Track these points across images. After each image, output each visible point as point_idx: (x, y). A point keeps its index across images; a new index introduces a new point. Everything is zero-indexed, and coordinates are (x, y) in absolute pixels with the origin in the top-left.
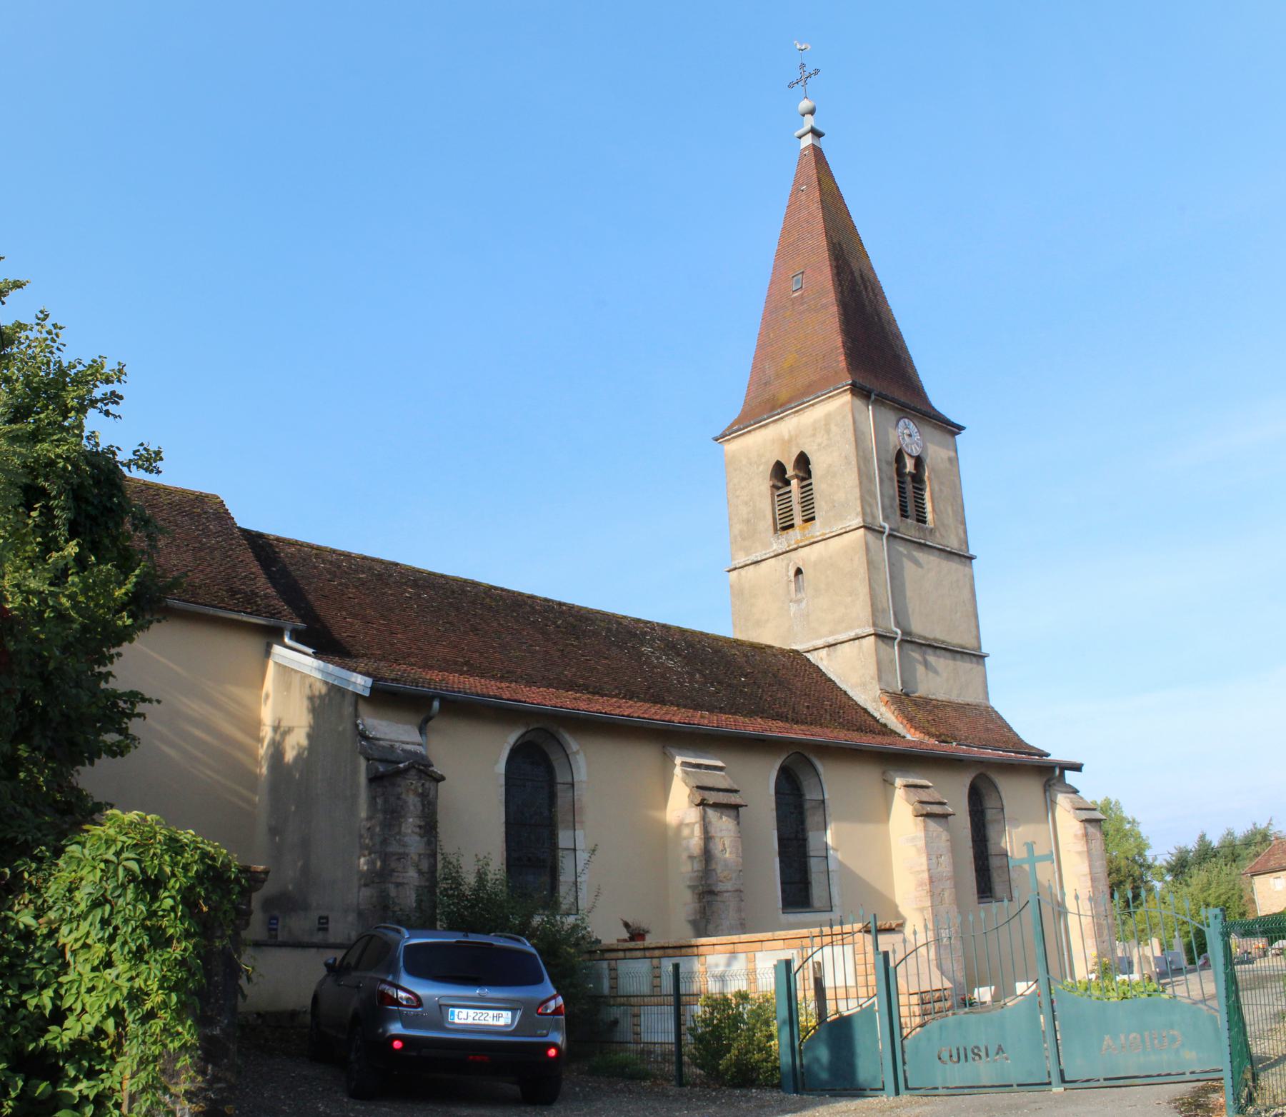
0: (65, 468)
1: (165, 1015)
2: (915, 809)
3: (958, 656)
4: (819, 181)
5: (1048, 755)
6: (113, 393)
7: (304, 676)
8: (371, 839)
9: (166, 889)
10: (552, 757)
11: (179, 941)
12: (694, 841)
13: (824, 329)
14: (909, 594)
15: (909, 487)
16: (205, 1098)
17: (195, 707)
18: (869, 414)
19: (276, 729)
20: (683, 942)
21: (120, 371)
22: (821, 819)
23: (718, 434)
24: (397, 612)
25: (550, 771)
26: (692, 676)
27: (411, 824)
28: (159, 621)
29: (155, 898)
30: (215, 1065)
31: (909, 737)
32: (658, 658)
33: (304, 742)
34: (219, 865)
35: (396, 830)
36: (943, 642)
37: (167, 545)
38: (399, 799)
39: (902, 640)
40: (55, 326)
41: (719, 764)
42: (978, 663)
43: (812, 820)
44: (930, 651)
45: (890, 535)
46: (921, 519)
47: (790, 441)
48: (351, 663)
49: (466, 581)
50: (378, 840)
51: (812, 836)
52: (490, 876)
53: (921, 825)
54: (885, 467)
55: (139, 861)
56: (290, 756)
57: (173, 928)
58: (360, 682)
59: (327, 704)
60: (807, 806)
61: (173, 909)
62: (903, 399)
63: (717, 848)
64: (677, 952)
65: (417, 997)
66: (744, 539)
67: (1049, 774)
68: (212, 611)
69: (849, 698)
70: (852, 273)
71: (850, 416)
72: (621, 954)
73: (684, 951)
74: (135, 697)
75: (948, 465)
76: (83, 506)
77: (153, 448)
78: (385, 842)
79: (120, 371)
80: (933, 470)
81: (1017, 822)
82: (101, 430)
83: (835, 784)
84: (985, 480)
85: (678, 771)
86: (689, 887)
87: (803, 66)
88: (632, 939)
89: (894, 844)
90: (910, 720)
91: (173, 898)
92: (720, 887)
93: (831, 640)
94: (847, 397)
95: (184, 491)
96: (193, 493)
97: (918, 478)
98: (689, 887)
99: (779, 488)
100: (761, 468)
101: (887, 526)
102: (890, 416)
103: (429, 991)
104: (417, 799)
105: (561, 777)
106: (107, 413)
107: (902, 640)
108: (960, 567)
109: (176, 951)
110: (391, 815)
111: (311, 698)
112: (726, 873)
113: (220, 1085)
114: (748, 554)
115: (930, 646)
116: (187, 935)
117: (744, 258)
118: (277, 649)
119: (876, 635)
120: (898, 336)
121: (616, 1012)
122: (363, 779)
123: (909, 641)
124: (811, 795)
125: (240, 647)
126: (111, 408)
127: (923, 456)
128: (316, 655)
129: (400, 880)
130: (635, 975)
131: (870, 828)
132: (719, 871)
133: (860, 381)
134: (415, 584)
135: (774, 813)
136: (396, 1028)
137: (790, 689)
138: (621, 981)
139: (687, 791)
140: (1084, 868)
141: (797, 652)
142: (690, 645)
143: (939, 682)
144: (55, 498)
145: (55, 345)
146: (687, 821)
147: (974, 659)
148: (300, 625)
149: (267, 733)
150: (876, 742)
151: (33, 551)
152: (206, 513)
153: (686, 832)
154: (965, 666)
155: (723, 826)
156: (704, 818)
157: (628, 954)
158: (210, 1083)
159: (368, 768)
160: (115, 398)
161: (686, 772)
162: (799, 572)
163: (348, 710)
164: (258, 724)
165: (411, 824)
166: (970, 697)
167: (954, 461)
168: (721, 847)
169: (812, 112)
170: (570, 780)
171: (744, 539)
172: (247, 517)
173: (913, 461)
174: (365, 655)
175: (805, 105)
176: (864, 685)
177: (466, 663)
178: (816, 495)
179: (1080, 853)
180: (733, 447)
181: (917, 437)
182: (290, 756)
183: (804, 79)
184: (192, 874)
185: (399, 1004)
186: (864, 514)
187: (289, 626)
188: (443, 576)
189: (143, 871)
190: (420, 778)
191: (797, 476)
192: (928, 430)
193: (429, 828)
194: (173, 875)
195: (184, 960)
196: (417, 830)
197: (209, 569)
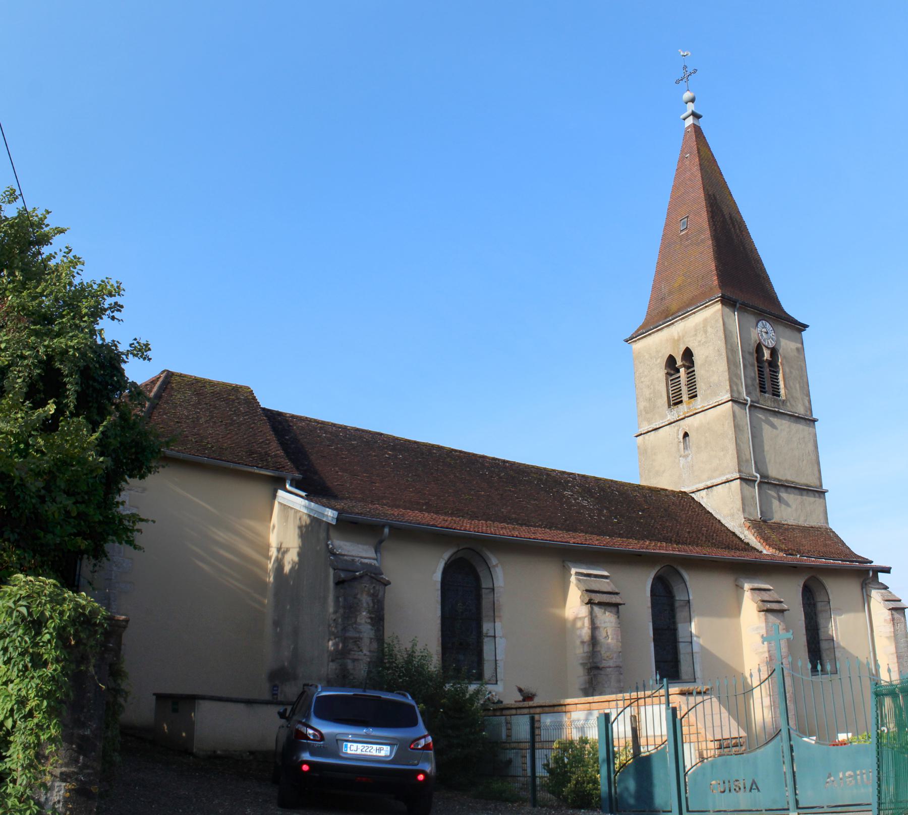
0: (74, 355)
1: (38, 717)
2: (758, 606)
3: (805, 493)
4: (698, 150)
5: (871, 562)
6: (116, 303)
7: (297, 511)
8: (336, 627)
9: (47, 628)
10: (479, 570)
11: (52, 664)
12: (585, 631)
13: (702, 258)
14: (766, 448)
15: (767, 370)
16: (76, 779)
17: (222, 536)
18: (734, 319)
19: (279, 550)
20: (555, 702)
21: (118, 287)
22: (687, 614)
23: (628, 337)
24: (377, 467)
25: (477, 579)
26: (600, 511)
27: (363, 617)
28: (163, 467)
29: (39, 633)
30: (85, 756)
31: (765, 552)
32: (575, 499)
33: (296, 559)
34: (87, 612)
35: (353, 620)
36: (793, 482)
37: (206, 422)
38: (355, 598)
39: (760, 481)
40: (75, 257)
41: (606, 573)
42: (820, 497)
43: (680, 615)
44: (783, 489)
45: (751, 406)
46: (776, 393)
47: (679, 340)
48: (333, 502)
49: (433, 446)
50: (340, 628)
51: (681, 627)
52: (417, 654)
53: (763, 618)
54: (747, 356)
55: (28, 608)
56: (287, 568)
57: (49, 653)
58: (330, 515)
59: (311, 531)
60: (677, 604)
61: (49, 641)
62: (761, 307)
63: (601, 635)
64: (551, 709)
65: (321, 733)
66: (647, 413)
67: (866, 575)
68: (232, 465)
69: (722, 525)
70: (723, 216)
71: (721, 320)
72: (514, 712)
73: (556, 708)
74: (136, 519)
75: (796, 354)
76: (91, 383)
77: (143, 342)
78: (344, 629)
79: (118, 287)
80: (784, 357)
81: (841, 611)
82: (110, 331)
83: (697, 587)
84: (826, 366)
85: (573, 579)
86: (582, 664)
87: (685, 67)
88: (524, 700)
89: (743, 632)
90: (766, 540)
91: (51, 634)
92: (604, 664)
93: (709, 484)
94: (719, 306)
95: (224, 384)
96: (230, 385)
97: (773, 364)
98: (582, 664)
99: (671, 375)
100: (659, 361)
101: (749, 399)
102: (752, 319)
103: (328, 729)
104: (369, 599)
105: (485, 584)
106: (113, 318)
107: (761, 482)
108: (806, 428)
109: (49, 671)
110: (349, 610)
111: (300, 527)
112: (608, 654)
113: (88, 771)
114: (649, 421)
115: (782, 486)
116: (57, 660)
117: (645, 214)
118: (281, 493)
119: (740, 478)
120: (759, 261)
121: (511, 754)
122: (331, 584)
123: (766, 482)
124: (680, 597)
125: (253, 493)
126: (116, 314)
127: (777, 347)
128: (307, 498)
129: (356, 657)
130: (521, 727)
131: (725, 621)
132: (603, 652)
133: (728, 294)
134: (393, 449)
135: (650, 610)
136: (306, 756)
137: (677, 520)
138: (513, 732)
139: (579, 593)
140: (892, 648)
141: (685, 492)
142: (602, 489)
143: (790, 512)
144: (67, 376)
145: (75, 271)
146: (580, 616)
147: (817, 495)
148: (297, 475)
149: (273, 553)
150: (727, 555)
151: (8, 403)
152: (238, 399)
153: (579, 624)
154: (809, 499)
155: (607, 619)
156: (591, 613)
157: (519, 711)
158: (81, 769)
159: (334, 574)
160: (118, 307)
161: (579, 580)
162: (686, 435)
163: (323, 535)
164: (268, 546)
165: (363, 617)
166: (814, 521)
167: (801, 351)
168: (604, 634)
169: (693, 100)
170: (491, 586)
171: (647, 413)
172: (267, 401)
173: (769, 352)
174: (349, 498)
175: (687, 95)
176: (732, 515)
177: (426, 504)
178: (698, 379)
179: (888, 638)
180: (639, 346)
181: (772, 334)
182: (287, 568)
183: (686, 78)
184: (66, 618)
185: (308, 739)
186: (732, 391)
187: (290, 476)
188: (416, 442)
189: (30, 614)
190: (372, 583)
191: (684, 366)
192: (781, 329)
193: (378, 619)
194: (51, 617)
195: (53, 677)
196: (369, 621)
197: (235, 437)
